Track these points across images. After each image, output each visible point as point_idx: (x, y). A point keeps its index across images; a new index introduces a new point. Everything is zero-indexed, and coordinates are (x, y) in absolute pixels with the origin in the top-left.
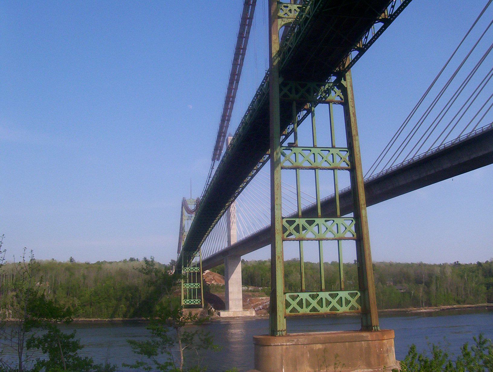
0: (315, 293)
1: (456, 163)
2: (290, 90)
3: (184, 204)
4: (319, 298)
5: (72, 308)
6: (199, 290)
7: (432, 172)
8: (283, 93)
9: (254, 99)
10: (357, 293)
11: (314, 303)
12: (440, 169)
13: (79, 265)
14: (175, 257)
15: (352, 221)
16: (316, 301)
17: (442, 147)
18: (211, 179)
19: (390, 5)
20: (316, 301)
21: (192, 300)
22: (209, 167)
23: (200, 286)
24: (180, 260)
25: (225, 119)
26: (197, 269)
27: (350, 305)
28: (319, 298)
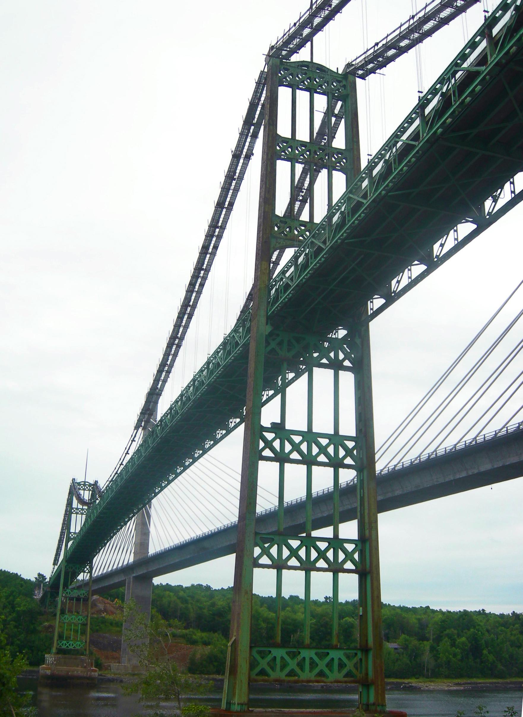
0: (295, 650)
1: (500, 464)
2: (280, 344)
3: (74, 489)
4: (300, 658)
5: (505, 639)
6: (84, 625)
7: (464, 474)
8: (269, 349)
9: (219, 348)
10: (356, 654)
11: (292, 664)
12: (476, 471)
13: (433, 611)
14: (48, 570)
15: (356, 545)
16: (296, 661)
17: (480, 439)
18: (128, 457)
19: (439, 243)
20: (296, 661)
21: (71, 642)
22: (128, 438)
23: (60, 619)
24: (56, 577)
25: (165, 368)
26: (82, 593)
27: (345, 671)
28: (300, 658)
